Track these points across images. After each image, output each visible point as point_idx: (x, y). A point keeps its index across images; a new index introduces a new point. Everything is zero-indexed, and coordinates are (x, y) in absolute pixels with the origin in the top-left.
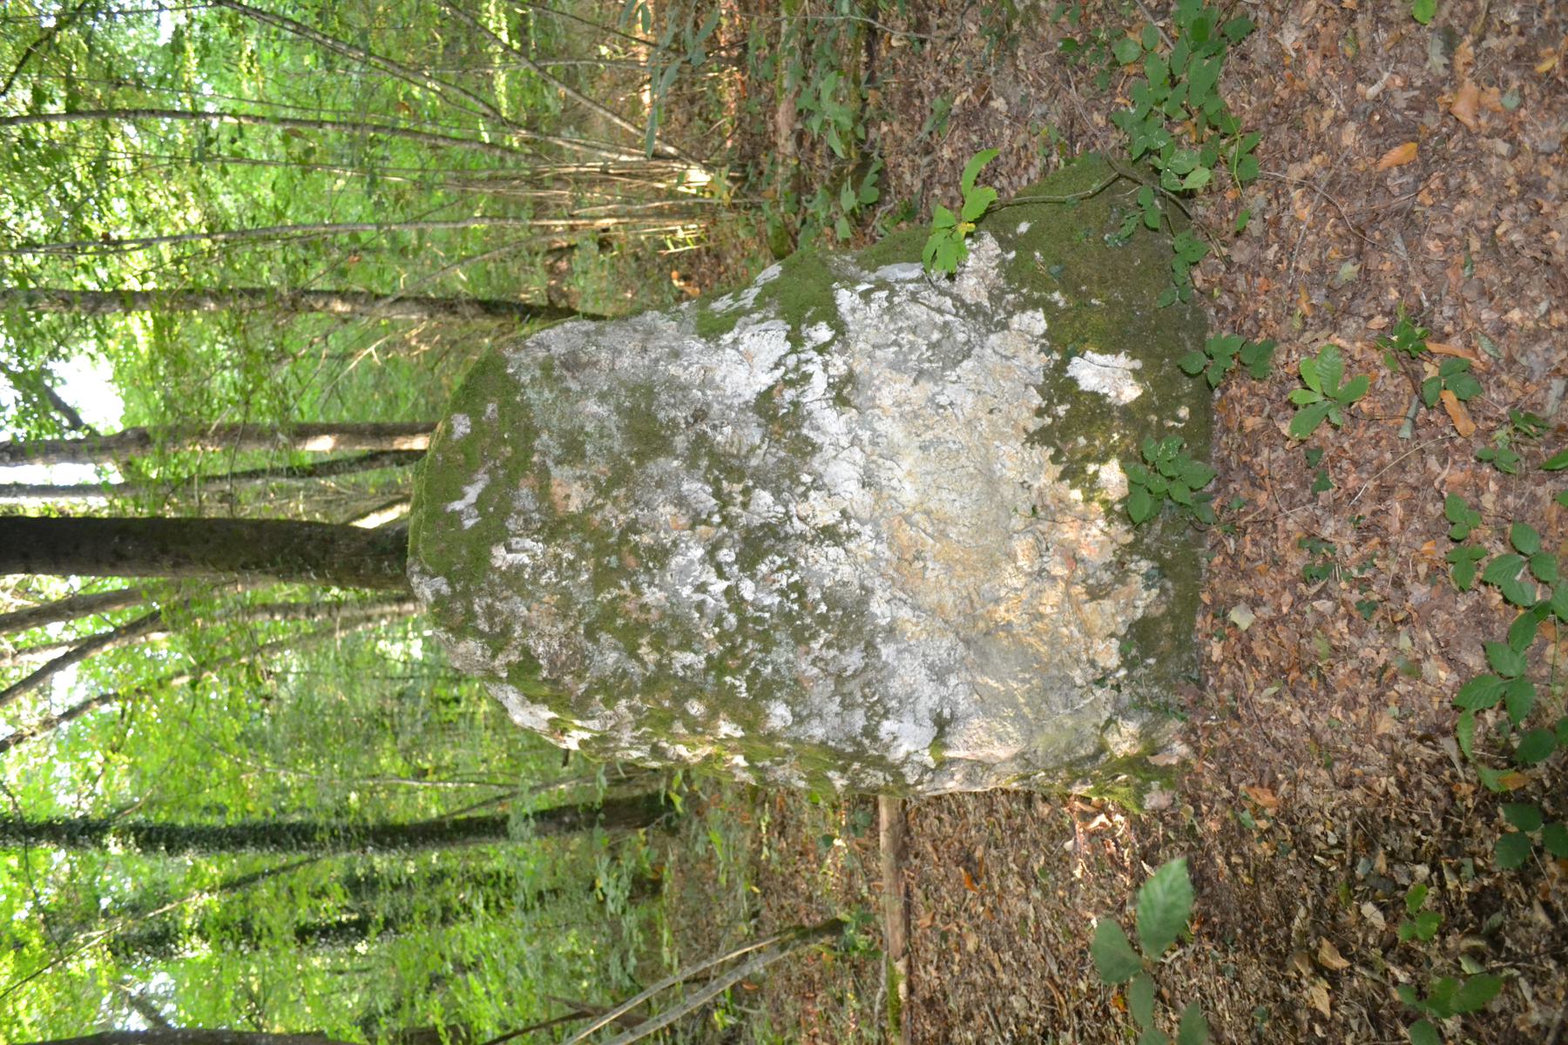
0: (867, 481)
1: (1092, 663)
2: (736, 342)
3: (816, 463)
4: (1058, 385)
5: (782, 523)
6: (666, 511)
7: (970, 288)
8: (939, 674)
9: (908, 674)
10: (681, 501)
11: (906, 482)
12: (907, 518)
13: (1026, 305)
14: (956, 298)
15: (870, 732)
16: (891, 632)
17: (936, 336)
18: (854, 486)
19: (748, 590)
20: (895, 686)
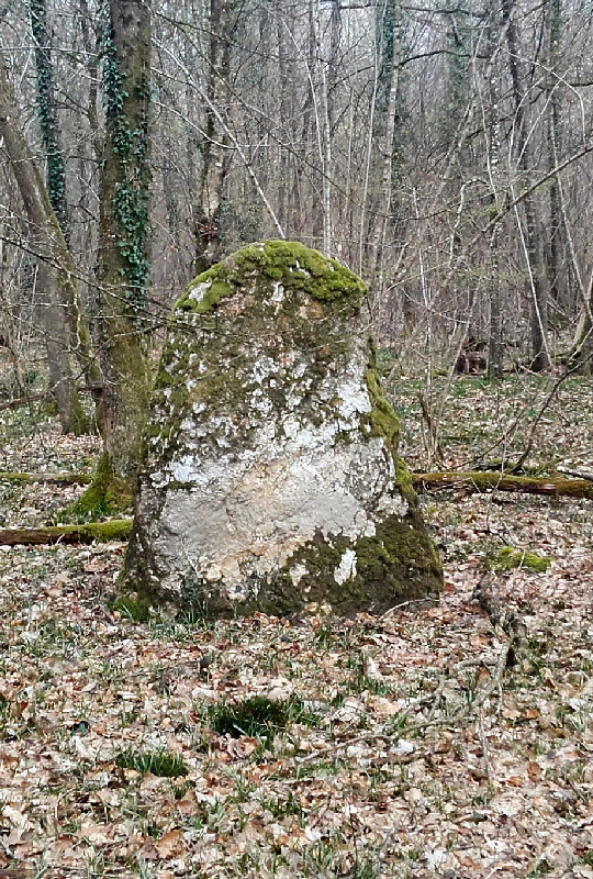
0: (303, 449)
1: (209, 566)
2: (363, 390)
3: (310, 426)
4: (342, 543)
5: (286, 409)
6: (293, 355)
7: (385, 500)
8: (212, 483)
9: (214, 470)
10: (296, 363)
11: (302, 469)
12: (284, 468)
13: (378, 527)
14: (380, 495)
15: (187, 452)
16: (234, 460)
17: (365, 483)
18: (300, 443)
19: (258, 392)
20: (209, 462)
